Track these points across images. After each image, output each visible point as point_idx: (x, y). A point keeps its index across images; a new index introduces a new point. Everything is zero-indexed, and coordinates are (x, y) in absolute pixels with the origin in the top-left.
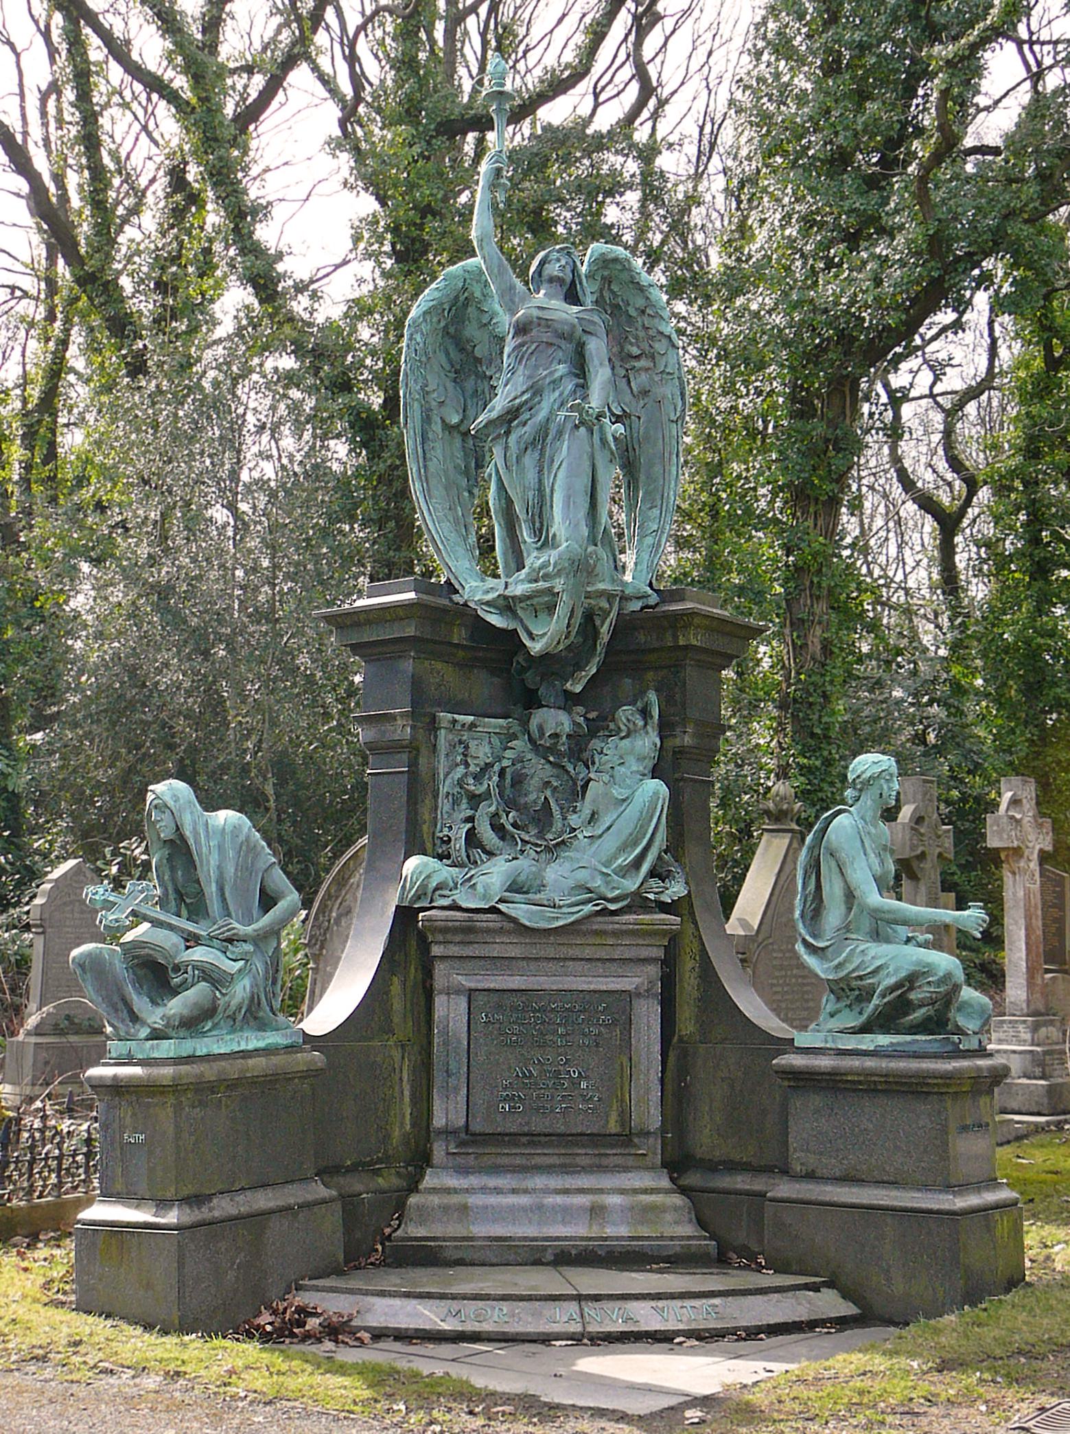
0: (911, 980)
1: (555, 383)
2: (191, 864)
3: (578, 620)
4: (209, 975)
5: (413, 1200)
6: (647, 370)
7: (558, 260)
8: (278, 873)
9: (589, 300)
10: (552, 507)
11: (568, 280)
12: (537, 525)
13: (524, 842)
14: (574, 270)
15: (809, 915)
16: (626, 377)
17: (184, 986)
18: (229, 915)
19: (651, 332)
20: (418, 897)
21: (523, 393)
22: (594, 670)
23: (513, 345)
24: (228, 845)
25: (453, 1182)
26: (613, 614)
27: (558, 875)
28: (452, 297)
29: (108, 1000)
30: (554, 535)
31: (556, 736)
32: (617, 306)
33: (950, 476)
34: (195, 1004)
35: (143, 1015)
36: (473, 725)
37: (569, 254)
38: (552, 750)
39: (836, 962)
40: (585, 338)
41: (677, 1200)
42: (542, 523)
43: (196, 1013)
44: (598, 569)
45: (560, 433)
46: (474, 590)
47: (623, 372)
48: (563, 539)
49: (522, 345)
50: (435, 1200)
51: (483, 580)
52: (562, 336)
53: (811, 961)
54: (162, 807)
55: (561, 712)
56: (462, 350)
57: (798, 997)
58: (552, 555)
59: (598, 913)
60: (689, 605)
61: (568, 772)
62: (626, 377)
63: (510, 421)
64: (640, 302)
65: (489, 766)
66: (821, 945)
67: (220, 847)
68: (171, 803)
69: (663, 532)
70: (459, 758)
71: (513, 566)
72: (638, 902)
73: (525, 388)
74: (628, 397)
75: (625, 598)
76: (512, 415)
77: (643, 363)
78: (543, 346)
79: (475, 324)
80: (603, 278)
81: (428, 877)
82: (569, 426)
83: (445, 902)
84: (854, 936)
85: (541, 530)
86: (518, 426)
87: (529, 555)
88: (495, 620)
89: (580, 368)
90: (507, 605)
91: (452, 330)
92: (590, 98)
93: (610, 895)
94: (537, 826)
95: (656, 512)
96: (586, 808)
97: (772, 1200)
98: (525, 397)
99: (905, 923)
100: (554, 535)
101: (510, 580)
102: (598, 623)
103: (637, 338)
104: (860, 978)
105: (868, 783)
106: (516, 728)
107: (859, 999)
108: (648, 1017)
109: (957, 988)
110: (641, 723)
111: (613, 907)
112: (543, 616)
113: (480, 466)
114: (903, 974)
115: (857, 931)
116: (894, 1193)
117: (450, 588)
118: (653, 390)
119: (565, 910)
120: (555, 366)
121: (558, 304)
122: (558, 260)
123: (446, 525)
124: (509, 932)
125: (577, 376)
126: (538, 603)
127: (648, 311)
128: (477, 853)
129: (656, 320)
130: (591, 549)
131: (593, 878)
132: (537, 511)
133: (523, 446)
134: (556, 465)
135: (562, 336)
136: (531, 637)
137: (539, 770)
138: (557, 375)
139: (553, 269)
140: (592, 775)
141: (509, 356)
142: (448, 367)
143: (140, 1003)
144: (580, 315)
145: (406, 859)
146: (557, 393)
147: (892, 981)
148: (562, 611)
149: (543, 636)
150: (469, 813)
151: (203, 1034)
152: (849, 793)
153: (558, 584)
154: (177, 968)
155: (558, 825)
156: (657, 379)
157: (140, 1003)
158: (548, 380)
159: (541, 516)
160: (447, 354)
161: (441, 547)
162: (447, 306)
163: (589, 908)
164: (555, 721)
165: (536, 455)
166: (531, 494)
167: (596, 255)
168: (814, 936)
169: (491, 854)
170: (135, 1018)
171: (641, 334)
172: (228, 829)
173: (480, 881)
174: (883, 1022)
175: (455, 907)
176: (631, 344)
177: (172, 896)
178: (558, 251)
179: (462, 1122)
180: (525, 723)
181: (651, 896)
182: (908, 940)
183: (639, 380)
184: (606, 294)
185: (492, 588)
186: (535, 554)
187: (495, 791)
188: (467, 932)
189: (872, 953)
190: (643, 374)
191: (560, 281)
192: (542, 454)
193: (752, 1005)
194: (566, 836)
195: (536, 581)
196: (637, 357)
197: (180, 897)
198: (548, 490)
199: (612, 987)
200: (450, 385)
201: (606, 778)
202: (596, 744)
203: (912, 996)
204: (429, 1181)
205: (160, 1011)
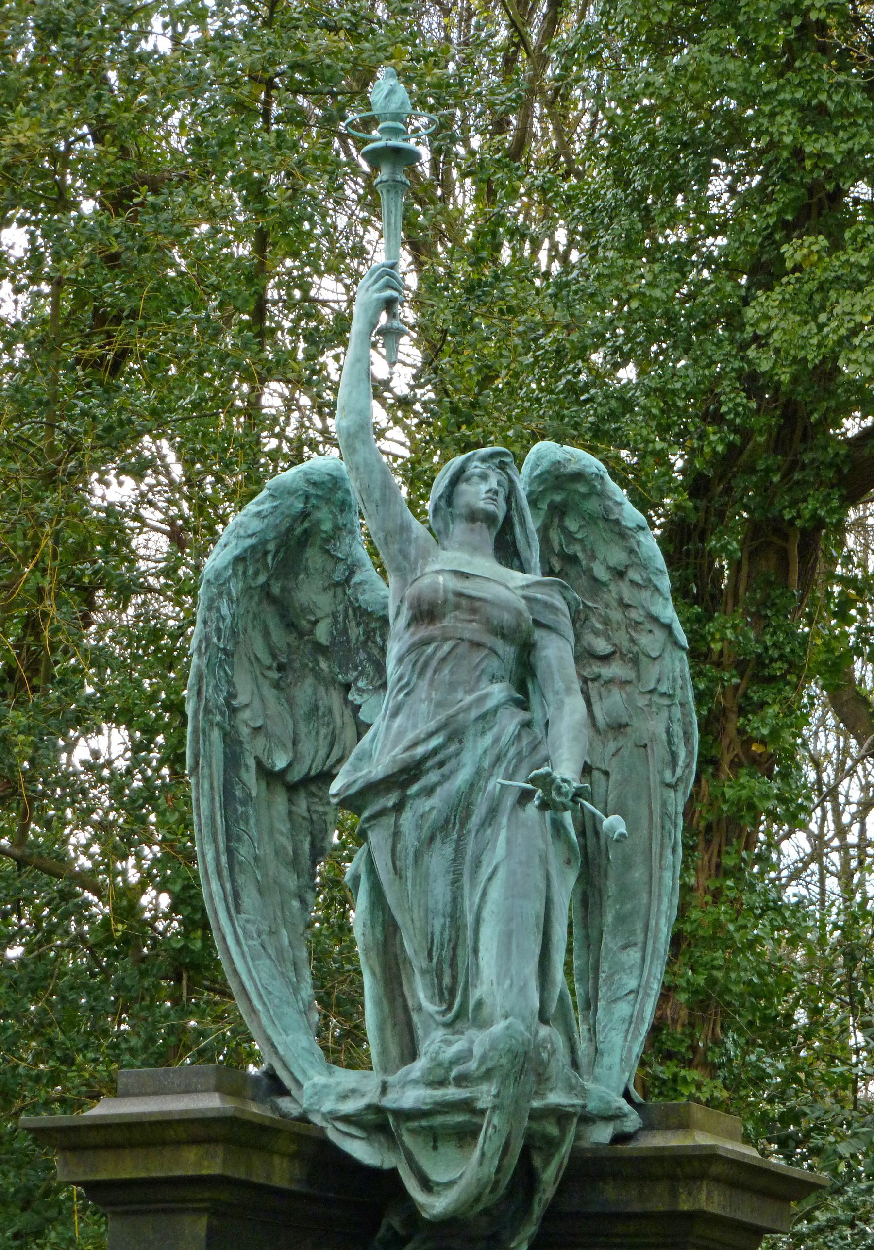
1: (486, 718)
3: (513, 1160)
6: (624, 683)
7: (484, 477)
10: (476, 951)
11: (501, 516)
12: (447, 980)
14: (511, 495)
19: (634, 615)
21: (431, 735)
23: (408, 639)
26: (565, 1149)
28: (283, 529)
30: (479, 1004)
32: (573, 560)
37: (502, 466)
40: (538, 635)
42: (454, 978)
45: (493, 812)
46: (321, 1092)
48: (499, 1012)
51: (331, 1074)
52: (500, 632)
56: (290, 626)
58: (478, 1041)
63: (405, 785)
64: (617, 556)
69: (647, 995)
71: (394, 1051)
73: (432, 725)
76: (406, 775)
77: (615, 670)
78: (463, 648)
79: (319, 583)
82: (509, 800)
85: (452, 991)
86: (418, 795)
87: (427, 1034)
88: (361, 1150)
90: (378, 1123)
91: (276, 590)
95: (634, 955)
98: (435, 742)
100: (479, 1004)
101: (391, 1079)
102: (537, 1161)
103: (606, 622)
112: (448, 1150)
117: (273, 1085)
118: (635, 723)
121: (485, 565)
123: (265, 964)
126: (444, 1126)
127: (634, 575)
129: (646, 595)
132: (446, 954)
133: (426, 832)
134: (485, 872)
135: (500, 632)
136: (427, 1185)
138: (490, 704)
141: (400, 660)
142: (266, 659)
144: (531, 593)
146: (488, 739)
148: (488, 1142)
153: (485, 1095)
156: (642, 702)
158: (474, 714)
159: (453, 965)
160: (266, 634)
161: (258, 1006)
162: (271, 547)
165: (448, 850)
166: (438, 923)
167: (545, 465)
171: (616, 615)
176: (596, 633)
178: (483, 460)
183: (607, 703)
186: (439, 1034)
190: (615, 690)
191: (489, 518)
192: (459, 851)
195: (442, 1083)
196: (605, 659)
198: (470, 919)
200: (270, 693)
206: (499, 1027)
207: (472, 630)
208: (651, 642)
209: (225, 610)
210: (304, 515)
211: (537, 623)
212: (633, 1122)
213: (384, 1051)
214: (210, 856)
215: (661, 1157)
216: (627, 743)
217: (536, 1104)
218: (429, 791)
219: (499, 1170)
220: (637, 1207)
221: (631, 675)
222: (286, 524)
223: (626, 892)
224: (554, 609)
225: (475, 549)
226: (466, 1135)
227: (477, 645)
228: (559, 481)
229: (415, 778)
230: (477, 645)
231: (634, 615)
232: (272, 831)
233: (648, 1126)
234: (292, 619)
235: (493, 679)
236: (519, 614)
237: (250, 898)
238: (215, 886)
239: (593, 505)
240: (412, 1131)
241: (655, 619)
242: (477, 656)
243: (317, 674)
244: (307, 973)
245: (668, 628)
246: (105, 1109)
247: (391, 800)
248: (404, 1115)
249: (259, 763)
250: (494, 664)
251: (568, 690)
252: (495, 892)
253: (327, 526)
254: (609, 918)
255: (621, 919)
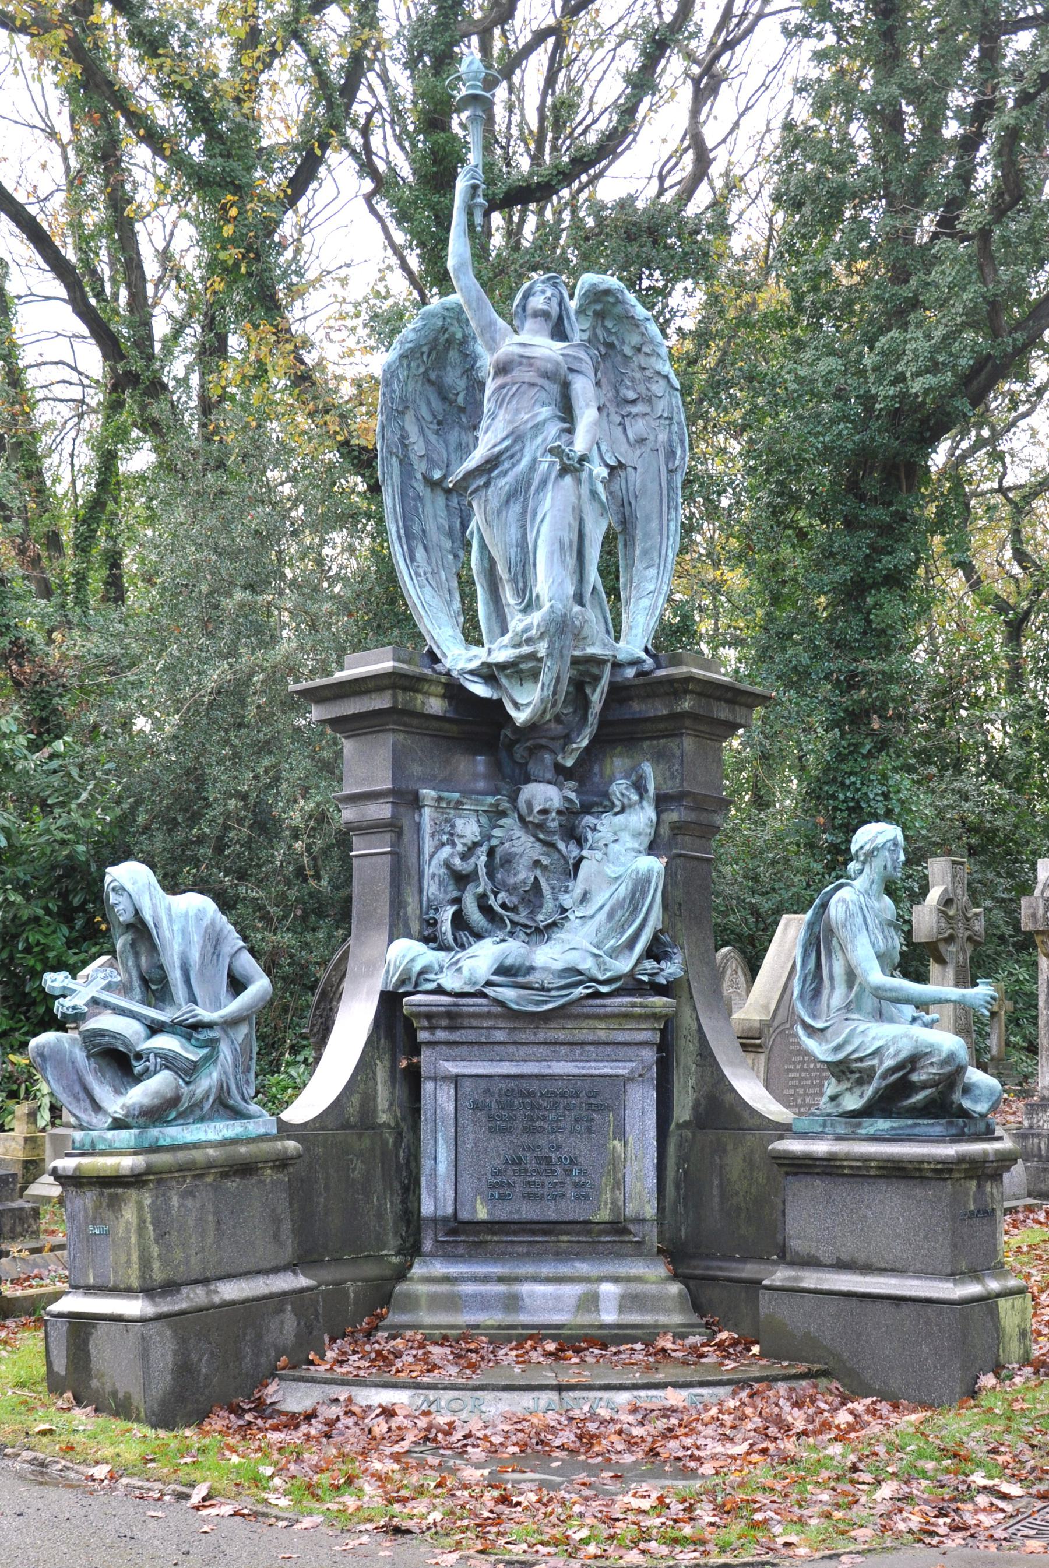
0: (913, 1061)
1: (538, 428)
2: (153, 948)
4: (169, 1061)
5: (401, 1288)
8: (246, 958)
9: (577, 337)
13: (514, 923)
14: (561, 303)
15: (808, 995)
16: (622, 424)
17: (146, 1074)
18: (195, 1002)
19: (648, 373)
20: (402, 982)
22: (586, 742)
24: (192, 929)
25: (439, 1268)
27: (549, 957)
29: (68, 1088)
31: (544, 812)
33: (1016, 570)
34: (157, 1093)
35: (104, 1104)
36: (459, 803)
38: (541, 826)
39: (834, 1043)
40: (571, 377)
41: (675, 1288)
43: (156, 1102)
44: (586, 631)
45: (544, 483)
47: (618, 419)
49: (502, 387)
50: (422, 1289)
53: (811, 1044)
54: (120, 890)
55: (550, 787)
56: (444, 399)
57: (789, 1075)
58: (536, 618)
59: (589, 996)
60: (684, 669)
61: (559, 851)
62: (622, 424)
64: (635, 339)
65: (476, 845)
66: (820, 1025)
67: (184, 932)
68: (128, 886)
70: (445, 838)
71: (497, 631)
72: (630, 985)
74: (624, 447)
75: (617, 665)
76: (491, 464)
78: (525, 387)
80: (596, 314)
81: (412, 960)
83: (432, 986)
84: (855, 1016)
85: (524, 591)
88: (480, 690)
89: (567, 412)
90: (489, 673)
91: (433, 376)
92: (655, 182)
93: (601, 978)
94: (527, 906)
95: (653, 571)
96: (578, 887)
97: (767, 1288)
99: (907, 1001)
102: (588, 691)
103: (633, 380)
104: (861, 1060)
105: (871, 855)
106: (505, 805)
107: (860, 1082)
108: (642, 1103)
109: (961, 1070)
110: (635, 797)
111: (604, 989)
113: (464, 526)
114: (903, 1055)
115: (859, 1009)
116: (893, 1281)
117: (433, 658)
119: (554, 993)
120: (538, 409)
122: (543, 292)
123: (428, 589)
124: (496, 1016)
125: (563, 420)
127: (645, 349)
128: (463, 936)
129: (653, 359)
130: (577, 608)
131: (584, 960)
132: (519, 569)
133: (503, 498)
135: (546, 375)
136: (517, 706)
137: (523, 845)
138: (539, 419)
139: (537, 302)
140: (585, 853)
142: (429, 418)
143: (103, 1093)
145: (391, 941)
146: (540, 439)
147: (889, 1063)
149: (525, 704)
150: (456, 894)
151: (168, 1123)
152: (853, 866)
154: (139, 1056)
155: (549, 905)
156: (654, 424)
157: (103, 1093)
160: (429, 403)
162: (425, 349)
163: (580, 991)
164: (544, 795)
166: (513, 551)
168: (814, 1017)
169: (479, 936)
170: (97, 1108)
171: (638, 375)
172: (192, 913)
173: (466, 965)
174: (884, 1104)
175: (440, 991)
177: (136, 983)
179: (450, 1210)
180: (513, 799)
181: (645, 978)
182: (914, 1020)
184: (600, 332)
185: (477, 656)
186: (520, 616)
187: (482, 871)
188: (453, 1019)
189: (872, 1034)
191: (545, 314)
193: (750, 1089)
194: (556, 917)
195: (519, 645)
196: (633, 402)
197: (145, 982)
199: (607, 1071)
201: (598, 855)
202: (589, 820)
203: (915, 1077)
204: (418, 1270)
205: (122, 1101)
206: (547, 606)
207: (530, 376)
208: (658, 388)
209: (396, 386)
210: (444, 330)
211: (571, 370)
212: (649, 663)
213: (490, 631)
214: (394, 530)
215: (670, 681)
216: (646, 449)
217: (576, 653)
218: (505, 473)
219: (554, 693)
220: (651, 714)
221: (648, 410)
222: (433, 335)
223: (647, 535)
224: (580, 360)
225: (536, 332)
226: (535, 675)
227: (533, 385)
228: (598, 296)
229: (495, 467)
230: (533, 385)
231: (648, 373)
232: (435, 516)
233: (659, 666)
234: (444, 395)
235: (543, 404)
236: (558, 364)
237: (420, 554)
238: (397, 547)
239: (618, 310)
240: (507, 676)
241: (659, 373)
242: (533, 391)
243: (461, 426)
244: (457, 595)
245: (666, 377)
246: (339, 676)
247: (481, 482)
248: (503, 666)
249: (424, 477)
250: (543, 395)
251: (587, 405)
252: (545, 529)
253: (459, 336)
254: (638, 552)
255: (645, 552)
